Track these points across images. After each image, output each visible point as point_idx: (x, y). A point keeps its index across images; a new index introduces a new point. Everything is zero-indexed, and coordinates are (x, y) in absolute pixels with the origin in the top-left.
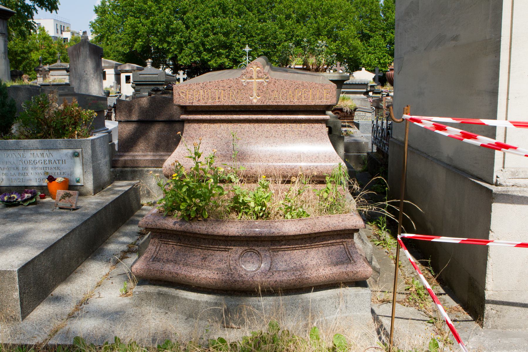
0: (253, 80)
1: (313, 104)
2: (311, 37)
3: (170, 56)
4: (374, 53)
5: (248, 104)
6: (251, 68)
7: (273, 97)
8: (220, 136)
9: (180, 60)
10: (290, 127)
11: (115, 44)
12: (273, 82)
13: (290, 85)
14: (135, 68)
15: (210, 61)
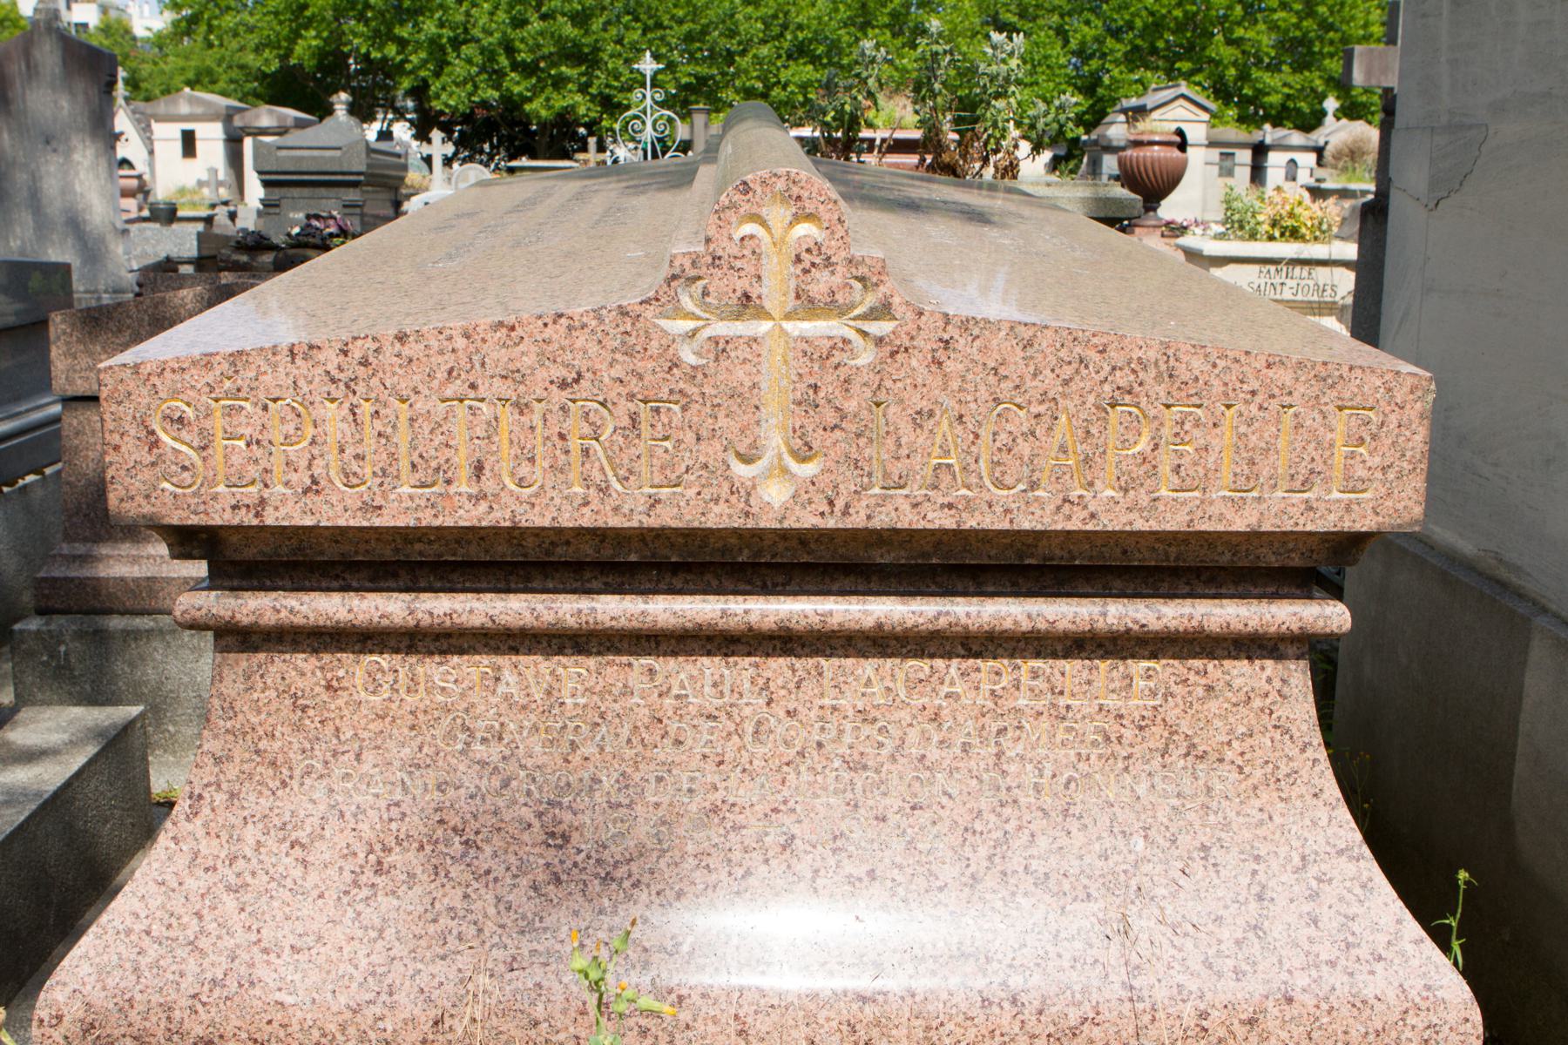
0: (764, 326)
1: (1240, 524)
2: (842, 32)
3: (406, 83)
4: (1031, 84)
5: (720, 517)
6: (749, 228)
8: (494, 752)
9: (438, 97)
10: (1040, 684)
11: (234, 45)
12: (925, 343)
13: (1067, 371)
14: (290, 122)
15: (530, 100)
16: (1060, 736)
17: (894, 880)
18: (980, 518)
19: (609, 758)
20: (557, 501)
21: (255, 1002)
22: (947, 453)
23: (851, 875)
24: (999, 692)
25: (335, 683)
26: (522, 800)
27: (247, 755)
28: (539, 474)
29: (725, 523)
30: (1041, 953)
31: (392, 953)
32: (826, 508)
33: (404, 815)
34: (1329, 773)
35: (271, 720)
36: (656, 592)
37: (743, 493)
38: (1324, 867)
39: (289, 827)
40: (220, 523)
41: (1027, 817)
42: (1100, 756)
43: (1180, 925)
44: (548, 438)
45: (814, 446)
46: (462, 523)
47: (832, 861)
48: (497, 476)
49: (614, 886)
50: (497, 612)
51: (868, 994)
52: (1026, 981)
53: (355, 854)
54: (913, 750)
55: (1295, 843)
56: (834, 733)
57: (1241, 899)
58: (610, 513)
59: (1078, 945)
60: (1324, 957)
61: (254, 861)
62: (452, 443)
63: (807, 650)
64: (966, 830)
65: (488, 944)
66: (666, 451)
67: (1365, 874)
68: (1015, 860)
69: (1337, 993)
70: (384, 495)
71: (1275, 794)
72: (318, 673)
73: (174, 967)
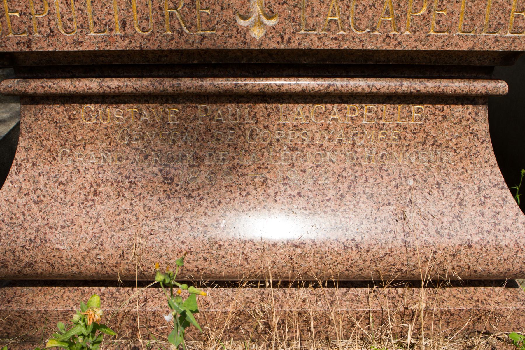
5: (232, 44)
7: (323, 21)
10: (372, 114)
16: (380, 136)
17: (308, 197)
18: (349, 44)
19: (189, 146)
20: (160, 38)
21: (48, 249)
22: (334, 15)
23: (291, 195)
24: (355, 118)
25: (72, 117)
26: (153, 164)
27: (38, 147)
28: (151, 25)
29: (235, 47)
30: (369, 227)
31: (102, 228)
32: (280, 40)
33: (105, 171)
34: (492, 153)
35: (47, 133)
36: (207, 76)
37: (242, 33)
38: (487, 192)
39: (58, 177)
40: (12, 51)
41: (365, 170)
42: (396, 145)
43: (427, 216)
44: (154, 9)
45: (274, 11)
46: (118, 49)
47: (283, 189)
48: (132, 27)
49: (192, 200)
50: (138, 86)
51: (298, 244)
52: (362, 238)
53: (85, 188)
54: (317, 142)
55: (476, 182)
56: (284, 135)
57: (452, 205)
58: (183, 43)
59: (384, 224)
60: (485, 229)
61: (44, 191)
62: (111, 12)
63: (272, 100)
64: (339, 176)
65: (141, 224)
66: (208, 14)
67: (504, 195)
68: (359, 189)
69: (490, 244)
70: (83, 37)
71: (469, 162)
72: (65, 113)
73: (14, 235)
